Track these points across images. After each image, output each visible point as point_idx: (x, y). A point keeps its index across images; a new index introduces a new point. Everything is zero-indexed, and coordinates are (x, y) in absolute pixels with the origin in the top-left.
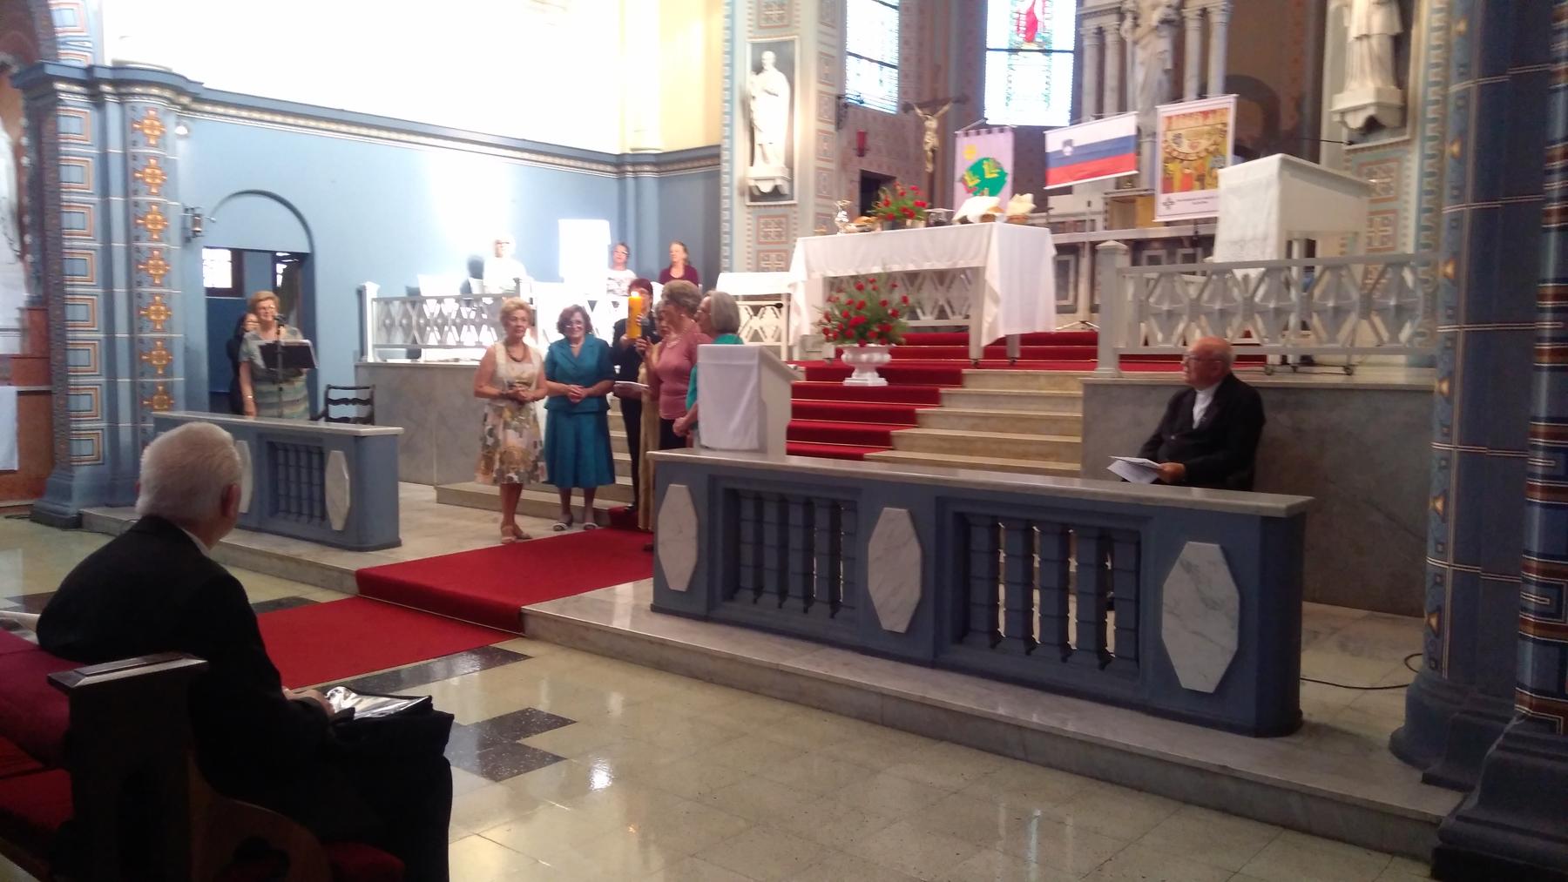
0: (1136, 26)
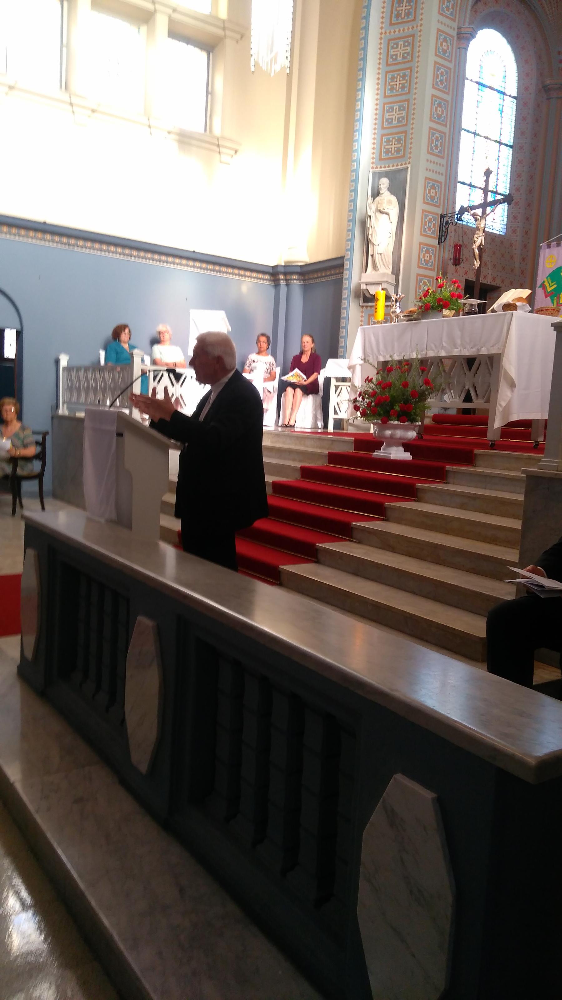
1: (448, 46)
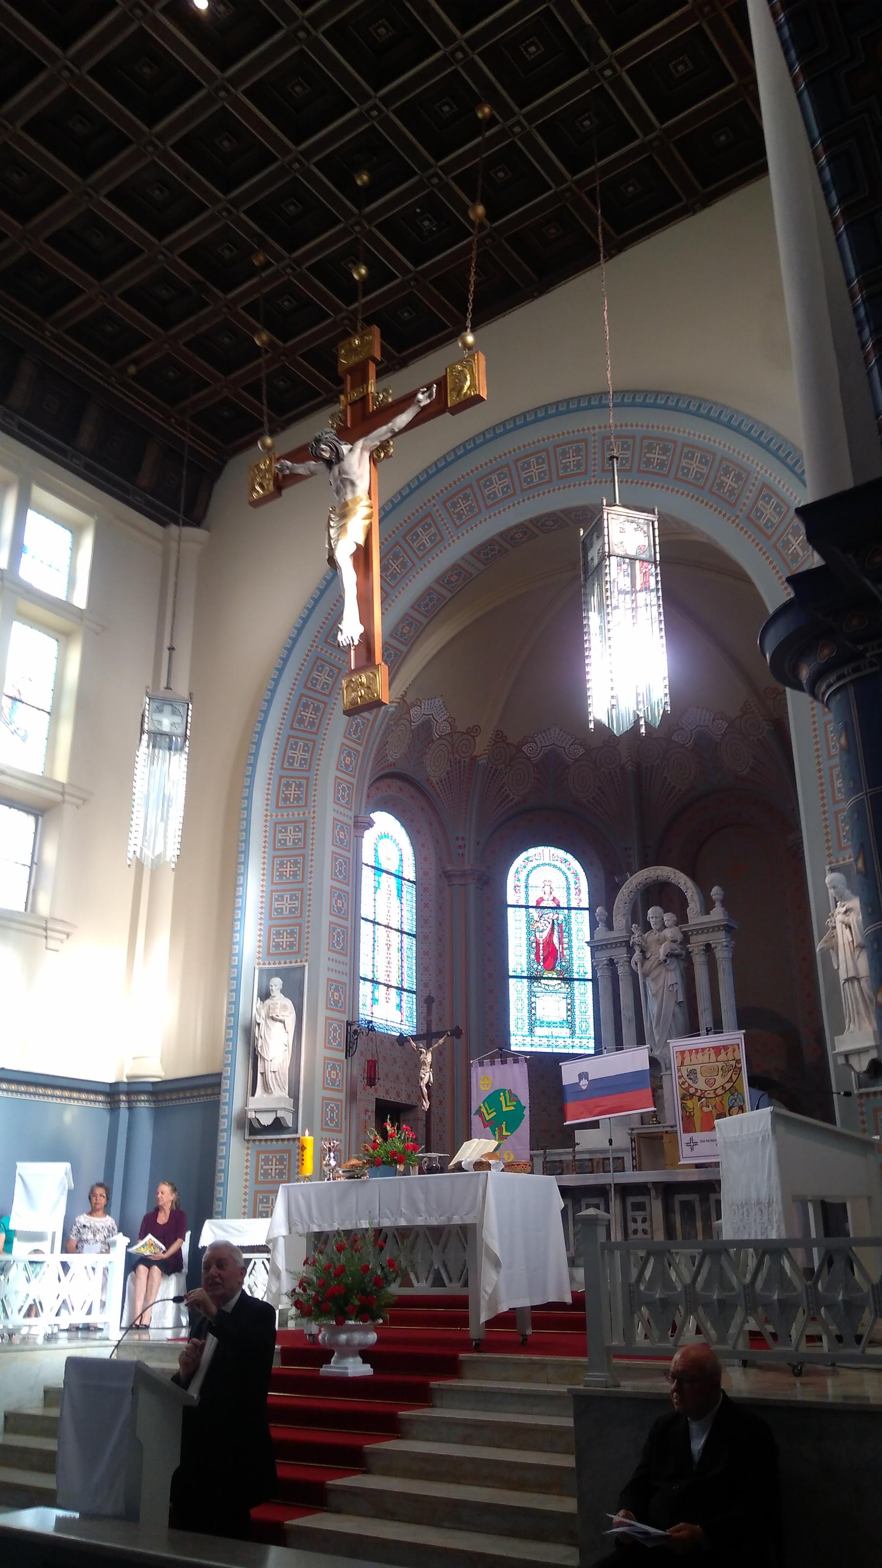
0: (645, 958)
1: (345, 835)
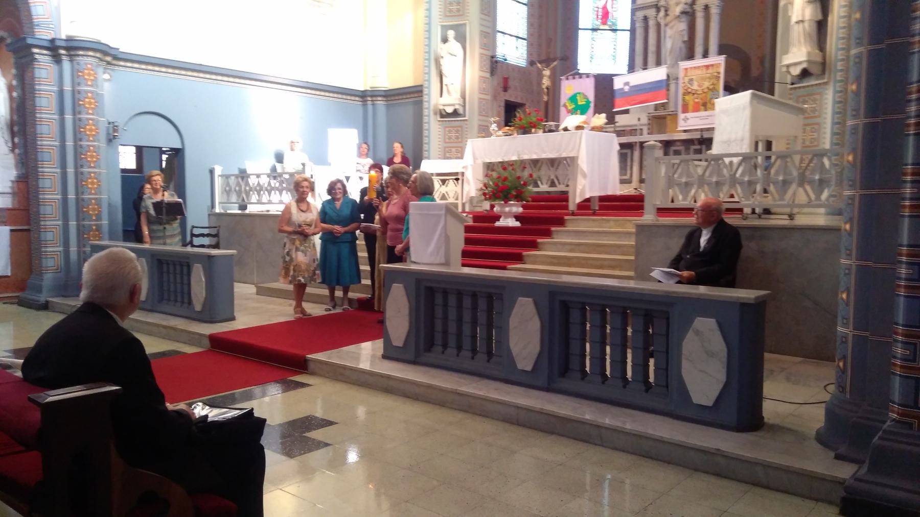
0: (667, 15)
